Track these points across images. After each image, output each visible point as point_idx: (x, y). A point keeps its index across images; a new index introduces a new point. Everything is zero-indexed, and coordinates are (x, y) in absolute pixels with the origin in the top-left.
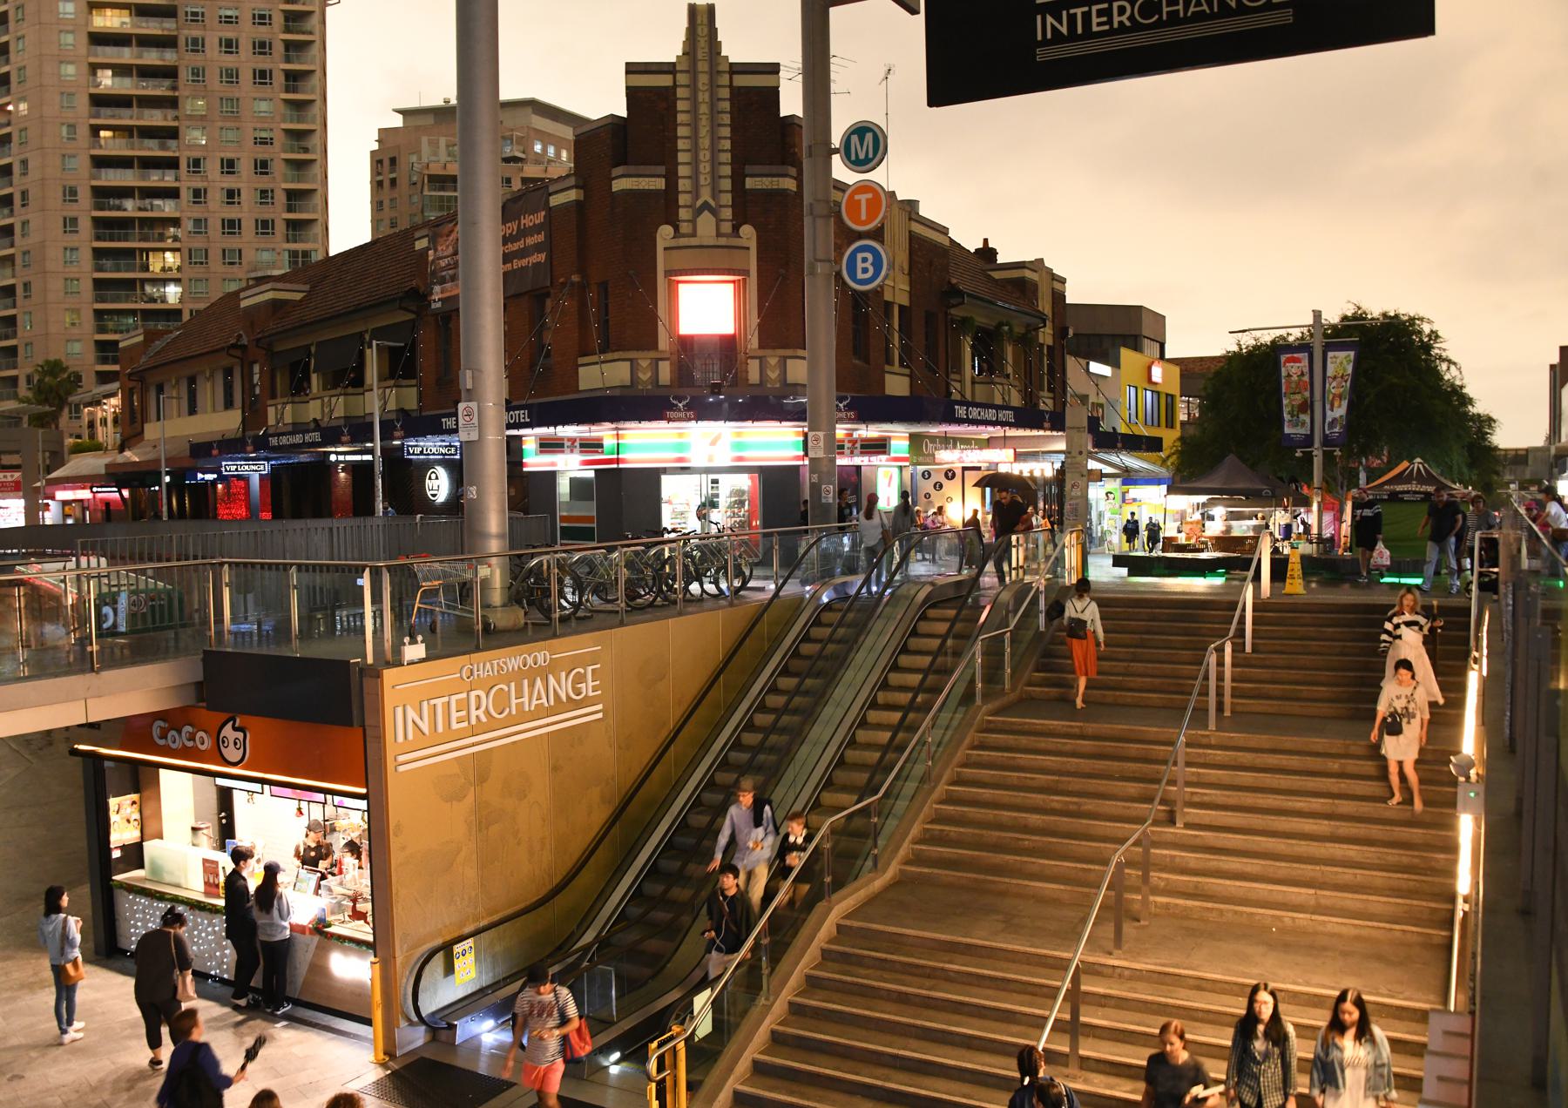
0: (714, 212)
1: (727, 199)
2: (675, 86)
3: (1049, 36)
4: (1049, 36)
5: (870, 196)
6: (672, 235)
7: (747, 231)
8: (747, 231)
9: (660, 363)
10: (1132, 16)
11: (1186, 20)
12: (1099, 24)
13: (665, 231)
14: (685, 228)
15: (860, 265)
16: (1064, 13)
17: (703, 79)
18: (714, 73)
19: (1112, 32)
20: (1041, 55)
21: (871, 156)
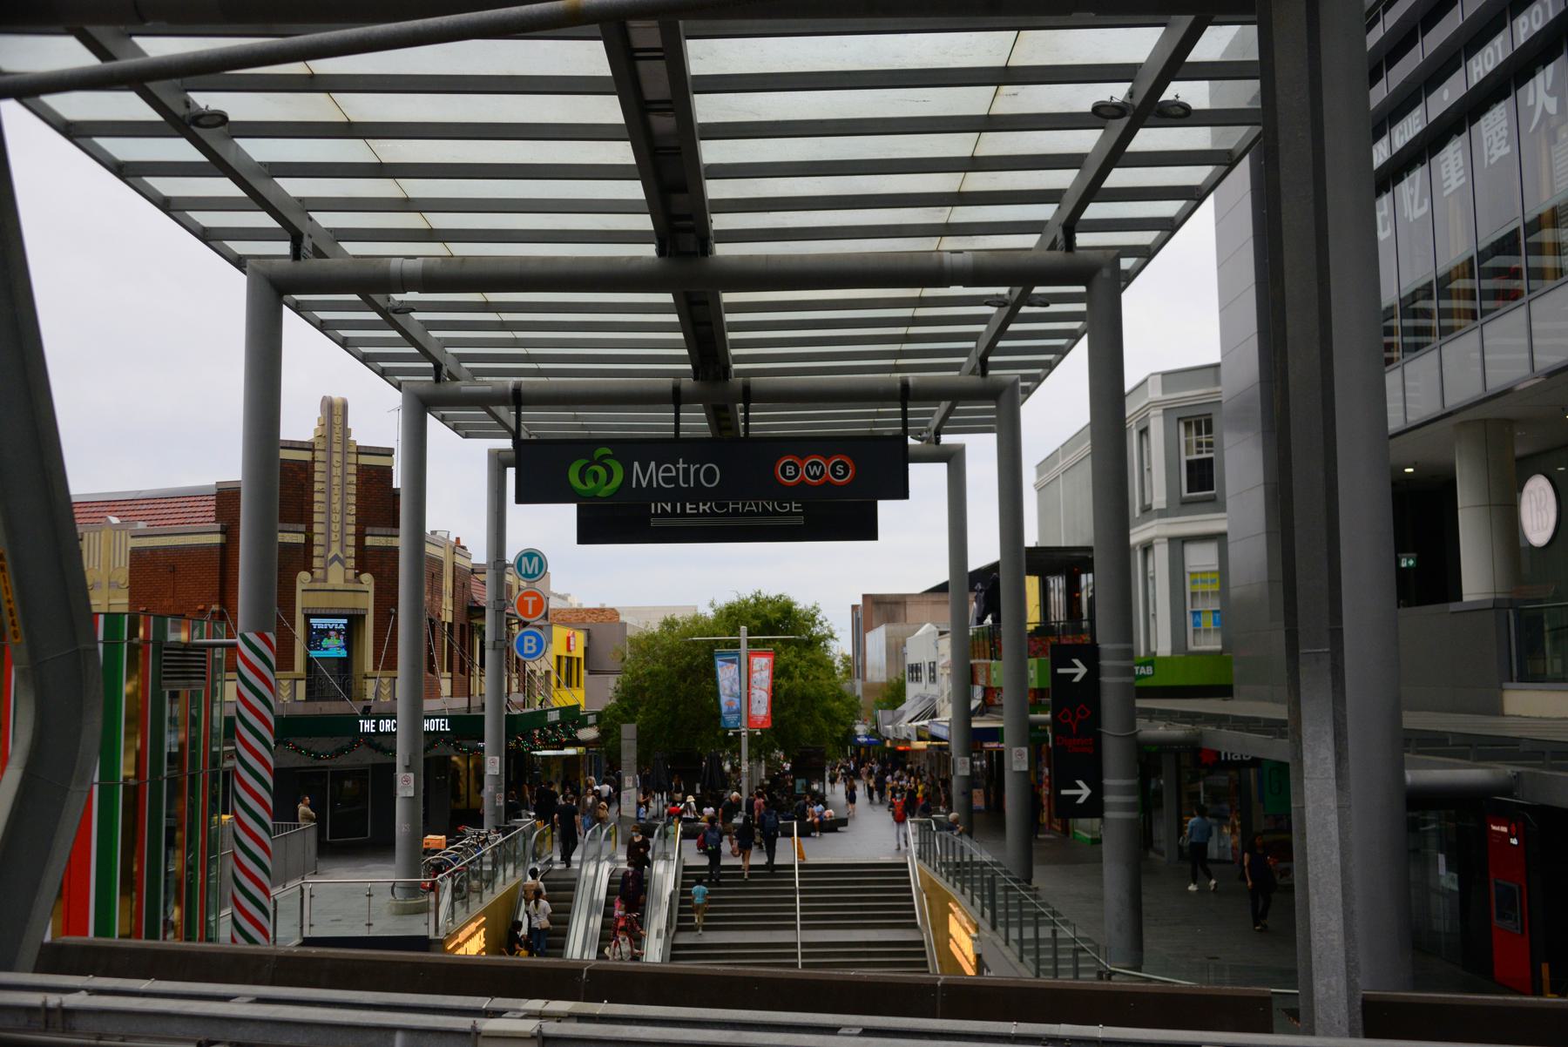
0: (342, 563)
1: (351, 552)
2: (313, 461)
3: (659, 511)
4: (659, 511)
5: (535, 598)
6: (309, 580)
7: (367, 578)
8: (367, 578)
9: (298, 682)
10: (711, 506)
11: (743, 514)
12: (691, 509)
13: (303, 576)
14: (318, 573)
15: (526, 644)
16: (692, 485)
17: (337, 458)
18: (345, 453)
19: (698, 515)
20: (654, 522)
21: (536, 572)
